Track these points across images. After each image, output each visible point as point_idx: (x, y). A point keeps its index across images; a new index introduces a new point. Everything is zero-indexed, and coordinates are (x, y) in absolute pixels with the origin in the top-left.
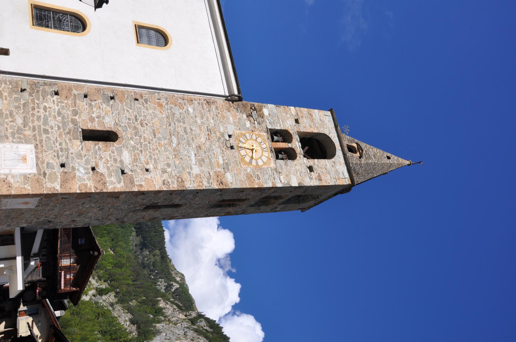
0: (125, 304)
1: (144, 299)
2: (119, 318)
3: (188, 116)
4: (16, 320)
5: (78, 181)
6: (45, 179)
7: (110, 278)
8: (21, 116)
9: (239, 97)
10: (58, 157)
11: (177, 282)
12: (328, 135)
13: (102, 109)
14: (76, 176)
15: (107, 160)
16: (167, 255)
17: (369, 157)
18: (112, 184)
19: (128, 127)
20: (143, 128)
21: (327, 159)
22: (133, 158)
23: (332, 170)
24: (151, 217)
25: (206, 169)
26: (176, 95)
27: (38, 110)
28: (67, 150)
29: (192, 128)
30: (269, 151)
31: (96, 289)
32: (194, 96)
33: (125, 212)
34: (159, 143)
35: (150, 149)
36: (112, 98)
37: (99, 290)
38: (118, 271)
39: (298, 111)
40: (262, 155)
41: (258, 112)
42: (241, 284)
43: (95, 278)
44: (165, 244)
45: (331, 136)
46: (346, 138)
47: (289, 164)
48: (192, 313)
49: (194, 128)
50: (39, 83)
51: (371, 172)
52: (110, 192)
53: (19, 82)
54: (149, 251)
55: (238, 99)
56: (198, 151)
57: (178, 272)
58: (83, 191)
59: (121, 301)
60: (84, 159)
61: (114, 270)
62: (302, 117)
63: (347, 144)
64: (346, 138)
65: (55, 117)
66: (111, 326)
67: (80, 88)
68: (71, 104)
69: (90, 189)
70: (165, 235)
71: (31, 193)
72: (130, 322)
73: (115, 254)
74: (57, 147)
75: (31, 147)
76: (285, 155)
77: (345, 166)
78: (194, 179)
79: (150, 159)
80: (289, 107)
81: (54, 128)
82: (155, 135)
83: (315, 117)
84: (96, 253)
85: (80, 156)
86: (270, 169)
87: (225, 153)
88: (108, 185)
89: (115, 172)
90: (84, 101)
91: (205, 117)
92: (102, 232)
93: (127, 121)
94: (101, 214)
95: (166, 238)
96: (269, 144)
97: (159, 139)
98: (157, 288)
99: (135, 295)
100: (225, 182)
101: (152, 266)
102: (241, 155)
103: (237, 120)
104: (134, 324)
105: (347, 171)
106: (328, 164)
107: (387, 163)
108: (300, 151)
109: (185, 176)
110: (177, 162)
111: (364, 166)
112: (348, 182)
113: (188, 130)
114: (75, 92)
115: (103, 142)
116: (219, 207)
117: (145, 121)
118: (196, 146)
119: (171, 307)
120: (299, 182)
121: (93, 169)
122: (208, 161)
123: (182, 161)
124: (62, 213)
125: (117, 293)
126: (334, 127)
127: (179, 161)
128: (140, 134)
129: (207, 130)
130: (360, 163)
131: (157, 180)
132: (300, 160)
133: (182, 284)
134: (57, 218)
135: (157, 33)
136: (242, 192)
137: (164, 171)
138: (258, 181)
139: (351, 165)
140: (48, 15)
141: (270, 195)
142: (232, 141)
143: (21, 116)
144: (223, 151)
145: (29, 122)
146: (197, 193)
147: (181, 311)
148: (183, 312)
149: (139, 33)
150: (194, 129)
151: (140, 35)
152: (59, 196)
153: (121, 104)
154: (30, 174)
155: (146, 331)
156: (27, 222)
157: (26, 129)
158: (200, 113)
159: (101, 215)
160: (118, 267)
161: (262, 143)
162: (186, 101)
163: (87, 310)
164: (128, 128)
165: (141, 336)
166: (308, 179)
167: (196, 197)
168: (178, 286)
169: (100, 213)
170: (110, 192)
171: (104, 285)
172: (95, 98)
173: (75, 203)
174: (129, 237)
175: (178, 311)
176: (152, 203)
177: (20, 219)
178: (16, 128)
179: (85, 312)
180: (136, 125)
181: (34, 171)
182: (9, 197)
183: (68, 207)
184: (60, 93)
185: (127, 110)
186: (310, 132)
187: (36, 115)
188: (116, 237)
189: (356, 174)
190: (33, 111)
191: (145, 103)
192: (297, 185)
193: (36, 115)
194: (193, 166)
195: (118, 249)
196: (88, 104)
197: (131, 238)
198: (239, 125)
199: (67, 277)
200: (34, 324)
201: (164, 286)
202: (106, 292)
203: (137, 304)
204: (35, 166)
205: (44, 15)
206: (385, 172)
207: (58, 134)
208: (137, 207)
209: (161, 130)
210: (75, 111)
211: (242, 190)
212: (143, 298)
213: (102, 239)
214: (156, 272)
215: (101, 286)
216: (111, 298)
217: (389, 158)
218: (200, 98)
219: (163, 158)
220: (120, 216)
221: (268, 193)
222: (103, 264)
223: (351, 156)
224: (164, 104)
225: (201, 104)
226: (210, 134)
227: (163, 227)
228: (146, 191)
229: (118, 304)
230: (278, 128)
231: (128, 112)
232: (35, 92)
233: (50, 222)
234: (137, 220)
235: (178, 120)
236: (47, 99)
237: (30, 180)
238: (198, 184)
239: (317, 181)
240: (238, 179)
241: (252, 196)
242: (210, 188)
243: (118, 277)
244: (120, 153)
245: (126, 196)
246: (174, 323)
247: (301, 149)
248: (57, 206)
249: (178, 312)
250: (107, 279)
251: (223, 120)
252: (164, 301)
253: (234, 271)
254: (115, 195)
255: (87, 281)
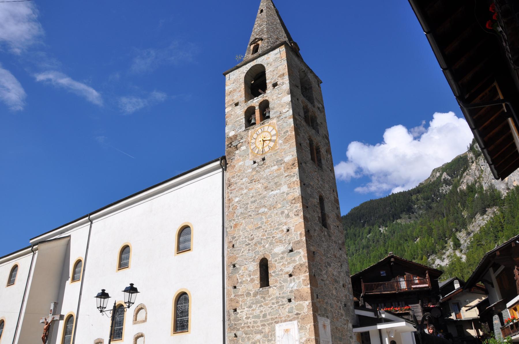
0: (466, 222)
1: (460, 204)
2: (481, 226)
3: (242, 201)
4: (464, 320)
5: (301, 287)
6: (301, 313)
7: (443, 238)
8: (255, 336)
9: (222, 160)
10: (283, 305)
11: (441, 175)
12: (245, 74)
13: (243, 273)
14: (297, 289)
15: (282, 265)
16: (416, 188)
17: (262, 31)
18: (301, 259)
19: (255, 250)
20: (255, 238)
21: (265, 71)
22: (279, 244)
23: (274, 65)
24: (337, 220)
25: (283, 180)
26: (226, 214)
27: (249, 323)
28: (277, 298)
29: (251, 196)
30: (263, 125)
31: (455, 250)
32: (225, 198)
33: (331, 243)
34: (266, 223)
35: (271, 230)
36: (234, 266)
37: (455, 247)
38: (435, 232)
39: (229, 104)
40: (267, 132)
41: (233, 141)
42: (434, 113)
43: (444, 252)
44: (405, 191)
45: (246, 71)
46: (247, 57)
47: (273, 106)
48: (470, 157)
49: (251, 194)
50: (229, 325)
51: (276, 26)
52: (308, 260)
53: (230, 339)
54: (414, 205)
55: (224, 160)
56: (269, 189)
57: (431, 175)
58: (309, 282)
59: (464, 225)
60: (284, 284)
61: (435, 235)
62: (233, 100)
63: (252, 55)
64: (247, 57)
65: (253, 310)
66: (489, 233)
67: (229, 292)
68: (242, 298)
69: (306, 276)
70: (397, 193)
71: (313, 323)
72: (484, 215)
73: (420, 236)
74: (275, 307)
75: (277, 326)
76: (267, 110)
77: (270, 53)
78: (292, 189)
79: (279, 229)
80: (226, 114)
81: (262, 310)
82: (260, 227)
83: (232, 89)
84: (392, 260)
85: (281, 288)
86: (278, 123)
87: (268, 165)
88: (302, 262)
89: (291, 257)
90: (239, 288)
91: (241, 186)
92: (400, 251)
93: (251, 252)
94: (335, 264)
95: (399, 191)
96: (258, 127)
97: (262, 223)
98: (448, 193)
99: (457, 214)
100: (292, 162)
101: (428, 201)
102: (269, 151)
103: (240, 158)
104: (486, 211)
105: (274, 51)
106: (269, 70)
107: (266, 12)
108: (261, 97)
109: (290, 197)
110: (279, 206)
111: (270, 34)
112: (283, 48)
113: (253, 199)
114: (232, 296)
115: (269, 270)
116: (321, 161)
117: (249, 237)
118: (265, 191)
119: (465, 178)
120: (287, 94)
121: (291, 275)
122: (276, 179)
123: (279, 202)
124: (335, 296)
125: (456, 231)
126: (238, 69)
127: (279, 204)
128: (260, 240)
129: (251, 184)
130: (267, 39)
131: (295, 222)
132: (268, 96)
133: (443, 170)
134: (341, 300)
135: (181, 235)
136: (300, 144)
137: (288, 216)
138: (289, 132)
139: (269, 47)
140: (180, 321)
141: (303, 118)
142: (258, 160)
143: (255, 336)
144: (267, 167)
145: (259, 329)
146: (304, 184)
147: (469, 168)
148: (470, 165)
149: (183, 249)
150: (252, 194)
151: (184, 249)
152: (315, 301)
153: (238, 258)
154: (298, 326)
155: (492, 199)
156: (346, 324)
157: (264, 331)
158: (239, 191)
159: (336, 263)
160: (431, 232)
161: (258, 133)
162: (231, 204)
163: (475, 256)
164: (256, 250)
165: (497, 203)
166: (284, 86)
167: (310, 184)
168: (445, 174)
169: (334, 264)
170: (308, 260)
171: (450, 243)
172: (235, 279)
173: (322, 287)
174: (403, 225)
175: (468, 171)
176: (319, 222)
177: (343, 329)
178: (264, 339)
179: (476, 258)
180: (253, 244)
181: (295, 322)
182: (318, 340)
183: (328, 293)
184: (234, 308)
185: (242, 253)
186: (245, 91)
187: (253, 324)
188: (403, 238)
189: (277, 40)
190: (250, 327)
191: (235, 239)
192: (290, 96)
193: (253, 324)
194: (282, 192)
195: (414, 234)
196: (241, 285)
197: (403, 223)
198: (245, 156)
199: (418, 282)
200: (468, 305)
201: (446, 186)
202: (457, 240)
203: (466, 211)
204: (292, 322)
205: (180, 324)
206: (275, 12)
207: (265, 307)
208: (324, 234)
209: (255, 223)
210: (247, 295)
211: (299, 146)
212: (460, 205)
213: (406, 250)
214: (433, 196)
215: (452, 246)
216: (462, 235)
217: (262, 11)
218: (226, 192)
219: (277, 218)
220: (336, 247)
221: (300, 120)
222: (430, 246)
223: (261, 49)
224: (235, 223)
225: (231, 192)
226: (255, 180)
227: (389, 195)
228: (305, 229)
229: (468, 228)
230: (243, 121)
231: (244, 252)
232: (235, 326)
233: (345, 305)
234: (340, 232)
235: (246, 210)
236: (240, 317)
237: (303, 325)
238: (296, 185)
239: (284, 78)
240: (289, 150)
241: (305, 134)
242: (298, 174)
243: (441, 231)
244: (276, 254)
245: (311, 246)
246: (482, 172)
247: (260, 96)
248: (326, 301)
249: (470, 171)
250: (444, 241)
251: (242, 170)
252: (461, 185)
253: (424, 122)
254: (311, 255)
255: (419, 265)
